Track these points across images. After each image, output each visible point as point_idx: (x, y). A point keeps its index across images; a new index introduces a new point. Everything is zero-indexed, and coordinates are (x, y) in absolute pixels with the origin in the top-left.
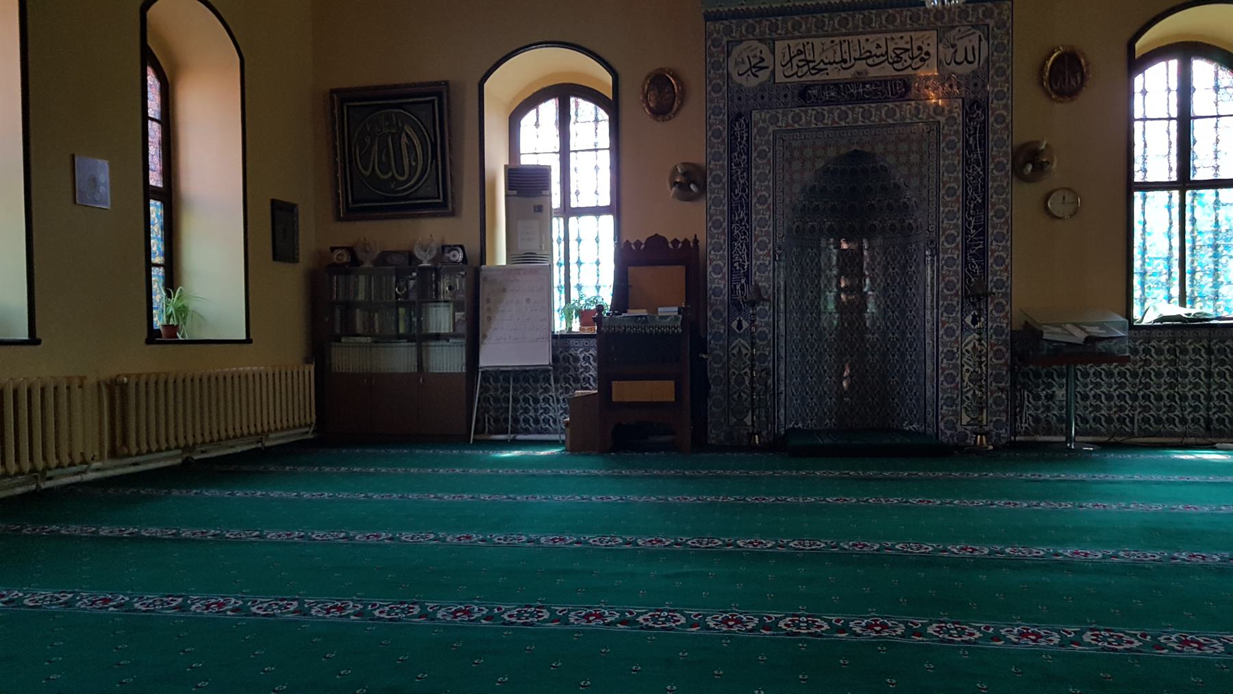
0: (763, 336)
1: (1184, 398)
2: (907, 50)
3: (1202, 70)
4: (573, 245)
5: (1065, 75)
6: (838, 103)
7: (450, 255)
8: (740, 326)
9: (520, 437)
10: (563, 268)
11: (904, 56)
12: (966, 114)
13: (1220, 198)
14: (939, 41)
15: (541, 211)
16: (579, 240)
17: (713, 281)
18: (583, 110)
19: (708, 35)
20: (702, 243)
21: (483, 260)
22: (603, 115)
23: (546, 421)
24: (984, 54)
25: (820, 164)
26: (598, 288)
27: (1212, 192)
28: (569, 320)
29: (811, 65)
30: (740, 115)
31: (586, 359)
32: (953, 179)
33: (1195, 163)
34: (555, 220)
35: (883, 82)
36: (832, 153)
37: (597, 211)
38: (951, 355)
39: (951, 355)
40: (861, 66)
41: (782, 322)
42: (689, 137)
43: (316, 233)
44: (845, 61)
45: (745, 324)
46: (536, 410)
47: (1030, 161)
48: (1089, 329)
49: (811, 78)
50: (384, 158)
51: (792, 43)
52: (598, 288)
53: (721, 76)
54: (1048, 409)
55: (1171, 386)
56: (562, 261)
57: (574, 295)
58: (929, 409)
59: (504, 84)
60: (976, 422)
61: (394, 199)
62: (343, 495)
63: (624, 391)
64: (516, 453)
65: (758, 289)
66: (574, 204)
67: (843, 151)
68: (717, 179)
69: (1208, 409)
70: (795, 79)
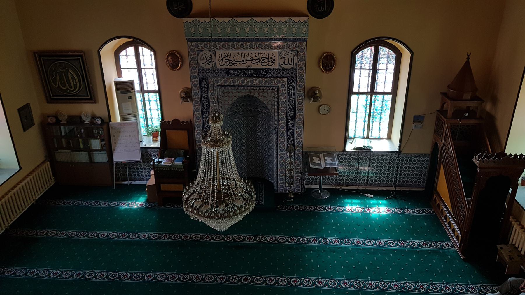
2: (267, 58)
3: (384, 51)
4: (147, 103)
5: (328, 62)
11: (266, 60)
14: (279, 55)
15: (132, 98)
17: (198, 138)
19: (189, 47)
21: (110, 121)
24: (295, 62)
27: (382, 96)
29: (230, 62)
30: (203, 79)
32: (283, 106)
35: (258, 70)
36: (239, 95)
38: (282, 165)
39: (282, 165)
40: (249, 63)
43: (38, 110)
44: (243, 61)
46: (138, 172)
47: (313, 94)
49: (230, 67)
50: (63, 82)
51: (222, 52)
53: (195, 64)
59: (107, 52)
63: (164, 187)
66: (145, 89)
67: (244, 94)
69: (368, 177)
70: (224, 66)
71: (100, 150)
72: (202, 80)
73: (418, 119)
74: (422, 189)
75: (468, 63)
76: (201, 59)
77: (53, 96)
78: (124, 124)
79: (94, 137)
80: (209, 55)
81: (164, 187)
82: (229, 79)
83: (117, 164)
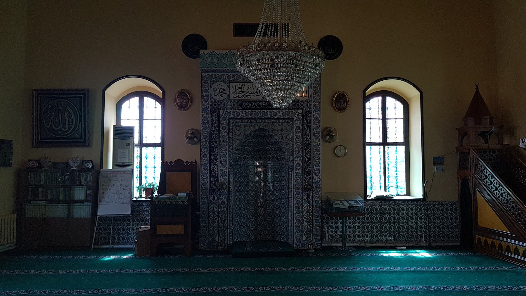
0: (223, 203)
1: (385, 228)
3: (390, 101)
5: (341, 102)
6: (254, 109)
7: (86, 165)
8: (214, 199)
9: (115, 246)
10: (139, 169)
12: (304, 116)
13: (397, 149)
15: (129, 145)
16: (147, 158)
18: (149, 102)
20: (198, 164)
21: (101, 167)
22: (159, 106)
23: (128, 239)
25: (247, 133)
26: (154, 178)
27: (394, 147)
28: (140, 192)
29: (244, 93)
30: (215, 112)
31: (147, 211)
33: (388, 136)
34: (135, 148)
36: (252, 128)
37: (155, 145)
41: (231, 196)
42: (193, 118)
44: (257, 93)
45: (216, 198)
48: (350, 202)
51: (237, 84)
52: (154, 178)
53: (208, 95)
54: (336, 232)
55: (381, 223)
56: (139, 166)
57: (143, 182)
58: (290, 234)
59: (113, 91)
60: (308, 239)
61: (61, 139)
62: (32, 272)
63: (162, 229)
64: (112, 257)
65: (221, 183)
66: (144, 142)
67: (257, 128)
68: (205, 137)
70: (237, 98)
71: (82, 202)
72: (213, 116)
73: (438, 161)
74: (459, 244)
75: (477, 94)
76: (214, 91)
77: (41, 139)
78: (117, 172)
79: (80, 185)
80: (223, 87)
81: (162, 229)
82: (242, 112)
83: (101, 218)
